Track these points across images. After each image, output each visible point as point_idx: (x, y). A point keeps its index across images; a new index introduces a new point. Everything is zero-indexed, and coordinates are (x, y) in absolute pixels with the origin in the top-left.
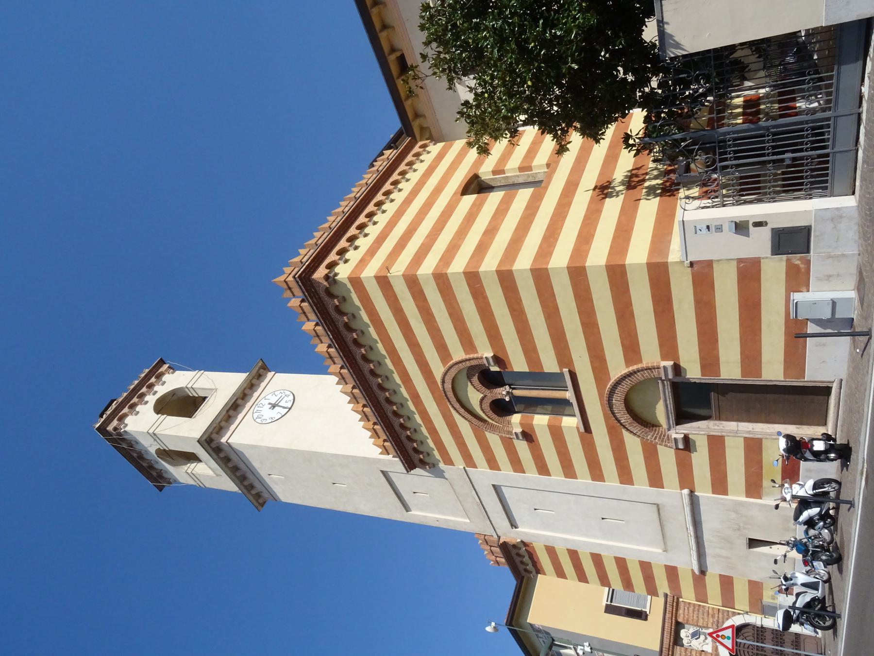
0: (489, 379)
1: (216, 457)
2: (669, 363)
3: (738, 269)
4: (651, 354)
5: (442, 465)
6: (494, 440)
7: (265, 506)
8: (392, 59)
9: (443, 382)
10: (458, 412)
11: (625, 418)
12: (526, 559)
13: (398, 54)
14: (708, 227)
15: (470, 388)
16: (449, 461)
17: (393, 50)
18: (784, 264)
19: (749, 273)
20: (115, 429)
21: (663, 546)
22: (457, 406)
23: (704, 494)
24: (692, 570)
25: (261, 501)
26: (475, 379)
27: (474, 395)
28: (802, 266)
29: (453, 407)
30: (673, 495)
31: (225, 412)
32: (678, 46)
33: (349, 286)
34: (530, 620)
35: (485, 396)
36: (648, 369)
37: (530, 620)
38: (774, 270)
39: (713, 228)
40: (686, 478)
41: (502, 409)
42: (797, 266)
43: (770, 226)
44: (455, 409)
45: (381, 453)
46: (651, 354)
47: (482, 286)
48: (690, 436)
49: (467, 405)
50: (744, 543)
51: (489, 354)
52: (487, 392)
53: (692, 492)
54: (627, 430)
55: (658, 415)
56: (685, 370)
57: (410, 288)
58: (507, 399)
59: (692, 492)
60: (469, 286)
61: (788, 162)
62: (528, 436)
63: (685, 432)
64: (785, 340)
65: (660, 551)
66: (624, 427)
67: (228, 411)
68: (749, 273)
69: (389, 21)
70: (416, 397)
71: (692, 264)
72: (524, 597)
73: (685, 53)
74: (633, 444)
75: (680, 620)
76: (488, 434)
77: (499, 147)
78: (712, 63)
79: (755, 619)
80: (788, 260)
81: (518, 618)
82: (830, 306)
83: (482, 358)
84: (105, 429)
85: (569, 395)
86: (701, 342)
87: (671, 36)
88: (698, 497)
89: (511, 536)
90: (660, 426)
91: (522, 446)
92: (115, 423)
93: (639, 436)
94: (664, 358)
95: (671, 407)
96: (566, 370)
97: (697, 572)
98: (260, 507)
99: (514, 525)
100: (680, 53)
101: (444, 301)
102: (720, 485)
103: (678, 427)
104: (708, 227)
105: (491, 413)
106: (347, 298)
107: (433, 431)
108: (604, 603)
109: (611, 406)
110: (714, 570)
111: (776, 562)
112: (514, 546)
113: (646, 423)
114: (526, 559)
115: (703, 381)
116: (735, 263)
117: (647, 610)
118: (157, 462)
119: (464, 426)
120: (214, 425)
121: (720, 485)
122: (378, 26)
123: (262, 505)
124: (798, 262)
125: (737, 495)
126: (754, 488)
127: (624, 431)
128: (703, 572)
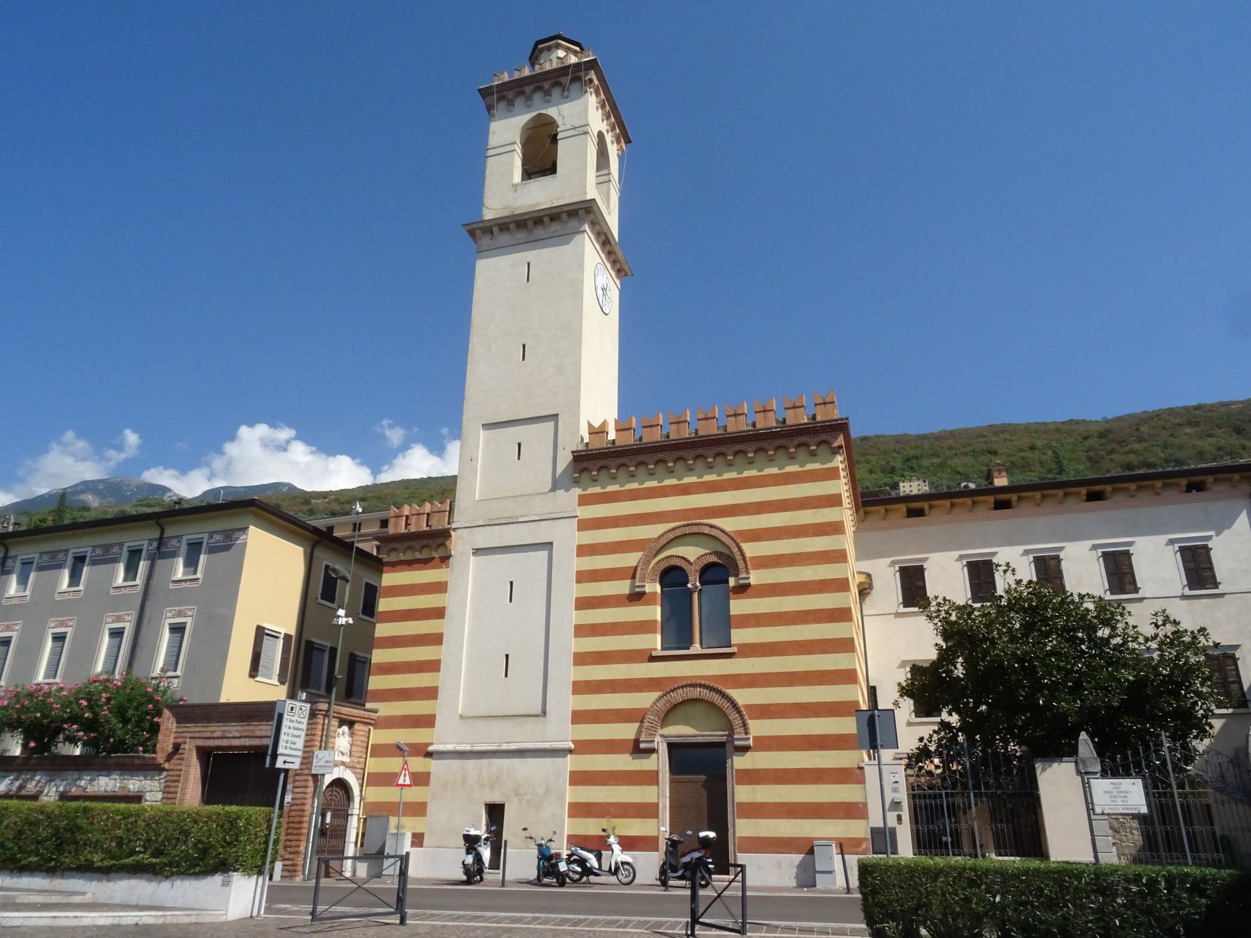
0: (721, 571)
1: (566, 209)
2: (751, 742)
4: (758, 728)
5: (577, 491)
9: (711, 526)
11: (678, 696)
12: (425, 555)
13: (926, 512)
15: (701, 551)
16: (584, 501)
17: (931, 507)
18: (862, 835)
19: (855, 811)
20: (591, 81)
25: (478, 232)
26: (714, 559)
27: (692, 553)
30: (560, 732)
32: (1044, 770)
33: (829, 465)
34: (252, 529)
36: (745, 725)
38: (858, 829)
41: (672, 576)
43: (898, 827)
44: (673, 529)
46: (758, 728)
49: (681, 540)
50: (496, 798)
51: (753, 581)
52: (698, 568)
53: (570, 751)
54: (661, 697)
57: (829, 524)
59: (570, 751)
61: (944, 839)
62: (636, 597)
68: (855, 811)
69: (956, 510)
71: (862, 768)
72: (274, 524)
74: (644, 700)
75: (356, 726)
76: (640, 554)
79: (356, 809)
80: (866, 839)
81: (257, 516)
83: (748, 573)
85: (696, 648)
89: (459, 544)
90: (662, 727)
96: (734, 649)
97: (431, 748)
99: (477, 552)
100: (1038, 771)
102: (579, 778)
107: (634, 496)
110: (434, 766)
113: (670, 714)
114: (425, 555)
116: (862, 800)
117: (258, 679)
119: (653, 531)
121: (579, 778)
123: (472, 233)
124: (864, 846)
125: (572, 794)
126: (580, 810)
128: (429, 755)
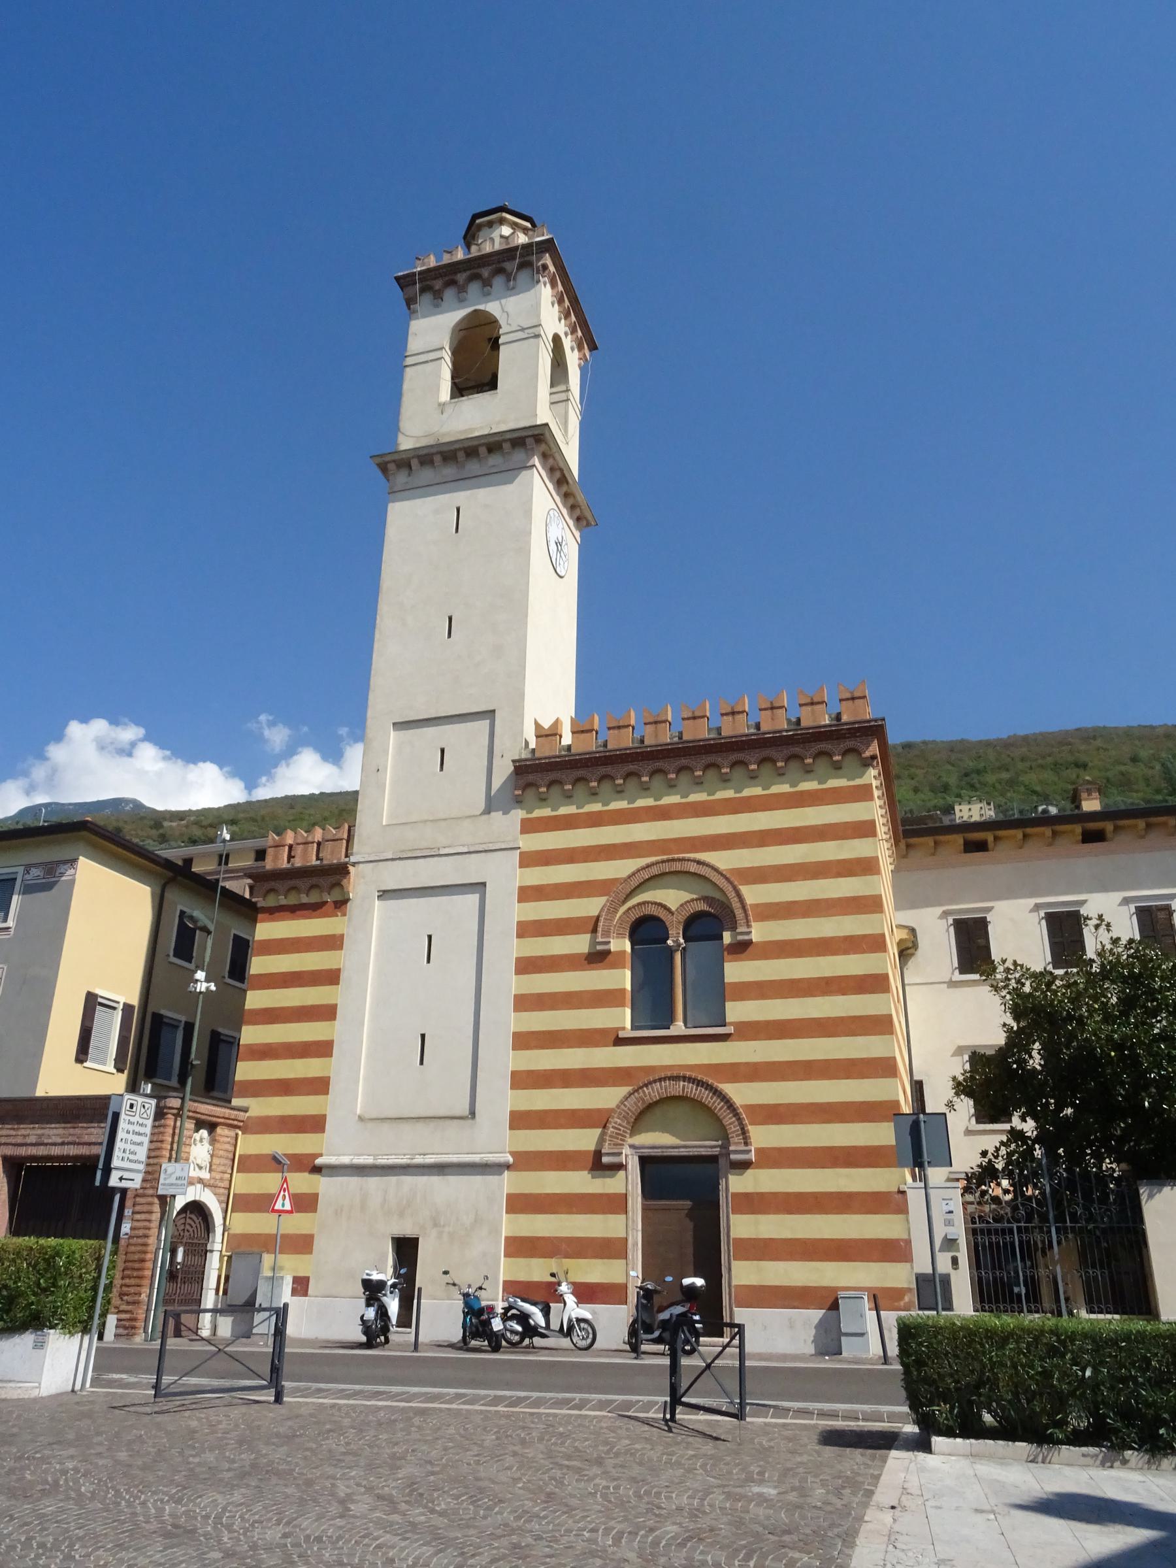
1: (508, 436)
3: (897, 1240)
4: (763, 1136)
5: (519, 814)
6: (592, 906)
7: (379, 473)
8: (989, 837)
10: (643, 868)
11: (654, 1093)
12: (314, 898)
14: (951, 1212)
15: (685, 896)
16: (528, 827)
19: (893, 1251)
20: (545, 267)
21: (367, 1116)
22: (655, 871)
23: (507, 1183)
24: (321, 1155)
25: (391, 466)
26: (702, 906)
27: (674, 899)
28: (902, 1303)
29: (657, 863)
30: (493, 1139)
31: (562, 465)
32: (1151, 1196)
34: (83, 861)
35: (672, 913)
37: (83, 861)
39: (949, 1216)
40: (525, 1161)
42: (902, 1298)
44: (648, 866)
45: (538, 725)
46: (763, 1136)
47: (864, 952)
48: (622, 1173)
50: (406, 1229)
51: (755, 937)
53: (508, 1167)
54: (630, 1094)
55: (643, 1135)
56: (742, 1174)
57: (859, 861)
58: (670, 942)
59: (508, 1167)
60: (865, 936)
61: (1016, 1290)
63: (630, 1167)
64: (796, 1287)
65: (358, 1112)
66: (637, 1091)
67: (561, 470)
68: (893, 1251)
70: (663, 814)
71: (904, 1193)
73: (1143, 1203)
74: (608, 1097)
75: (219, 1130)
77: (355, 754)
78: (1123, 1225)
79: (218, 1243)
80: (909, 1290)
82: (859, 1331)
83: (749, 926)
84: (547, 251)
86: (788, 1195)
87: (1160, 1191)
88: (501, 1174)
89: (361, 884)
91: (580, 944)
92: (552, 269)
93: (618, 1107)
94: (758, 1150)
95: (675, 1152)
96: (729, 1029)
97: (319, 1161)
98: (379, 460)
99: (384, 894)
100: (1144, 1198)
101: (840, 899)
102: (519, 1204)
103: (636, 1159)
104: (951, 1212)
105: (637, 914)
106: (840, 772)
108: (98, 991)
109: (676, 1078)
110: (324, 1185)
111: (446, 1273)
112: (338, 884)
113: (642, 1118)
115: (722, 1195)
116: (906, 1237)
117: (85, 1064)
118: (462, 301)
120: (554, 450)
121: (519, 1204)
122: (1029, 830)
123: (383, 468)
126: (519, 1247)
127: (629, 1089)
128: (317, 1170)
